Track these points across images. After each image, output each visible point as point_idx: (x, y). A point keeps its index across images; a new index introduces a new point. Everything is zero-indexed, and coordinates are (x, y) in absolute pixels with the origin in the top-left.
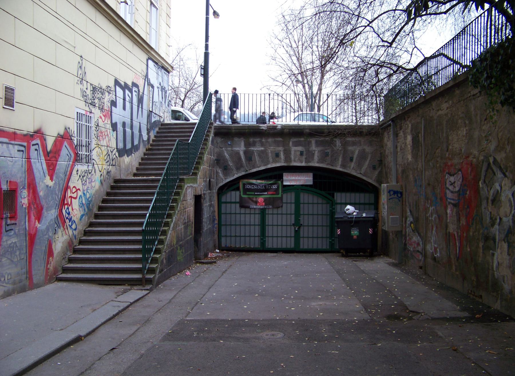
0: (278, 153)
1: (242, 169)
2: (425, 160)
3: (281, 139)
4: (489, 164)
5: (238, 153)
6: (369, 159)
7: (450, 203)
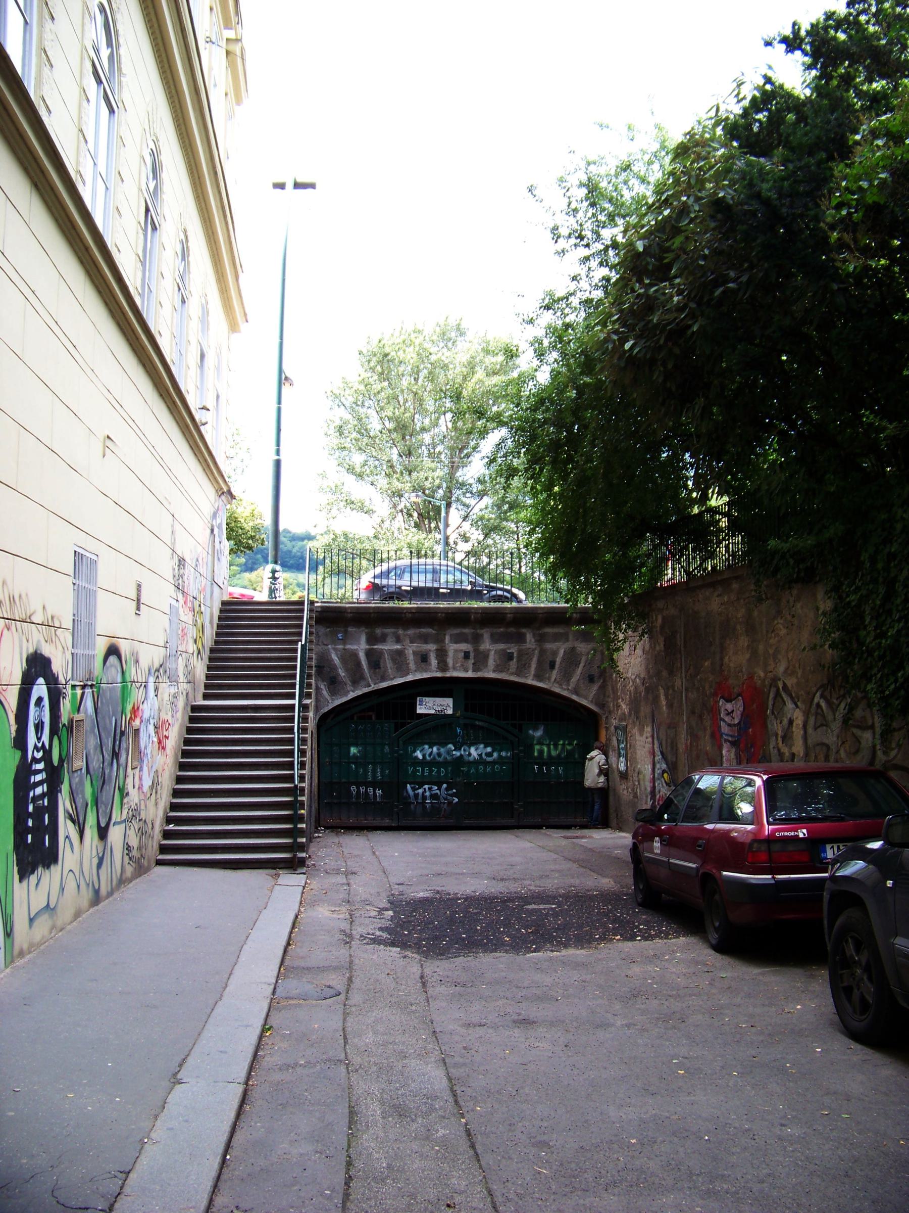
0: (426, 655)
1: (363, 683)
2: (686, 675)
3: (430, 630)
4: (778, 689)
5: (354, 655)
6: (582, 665)
7: (726, 741)
